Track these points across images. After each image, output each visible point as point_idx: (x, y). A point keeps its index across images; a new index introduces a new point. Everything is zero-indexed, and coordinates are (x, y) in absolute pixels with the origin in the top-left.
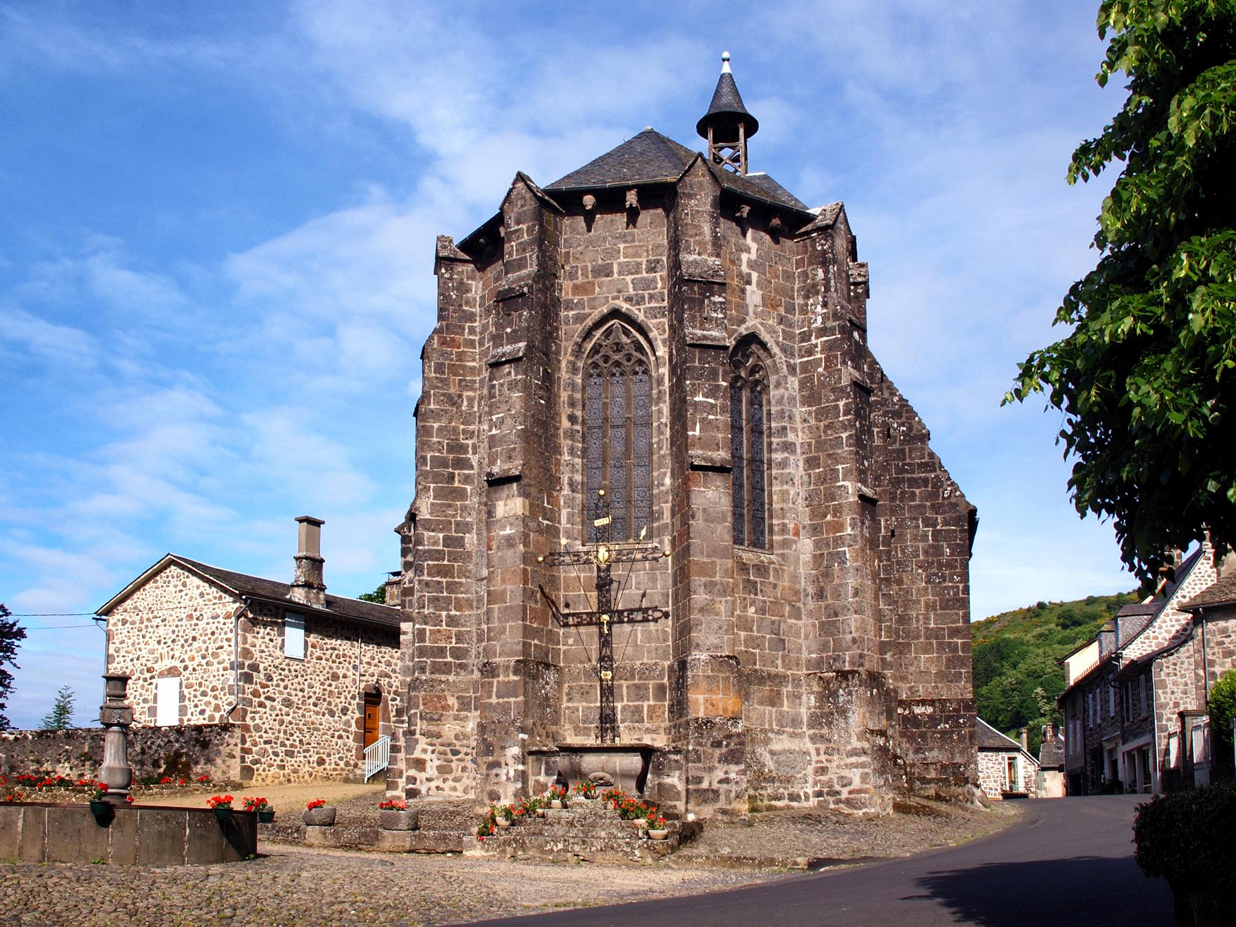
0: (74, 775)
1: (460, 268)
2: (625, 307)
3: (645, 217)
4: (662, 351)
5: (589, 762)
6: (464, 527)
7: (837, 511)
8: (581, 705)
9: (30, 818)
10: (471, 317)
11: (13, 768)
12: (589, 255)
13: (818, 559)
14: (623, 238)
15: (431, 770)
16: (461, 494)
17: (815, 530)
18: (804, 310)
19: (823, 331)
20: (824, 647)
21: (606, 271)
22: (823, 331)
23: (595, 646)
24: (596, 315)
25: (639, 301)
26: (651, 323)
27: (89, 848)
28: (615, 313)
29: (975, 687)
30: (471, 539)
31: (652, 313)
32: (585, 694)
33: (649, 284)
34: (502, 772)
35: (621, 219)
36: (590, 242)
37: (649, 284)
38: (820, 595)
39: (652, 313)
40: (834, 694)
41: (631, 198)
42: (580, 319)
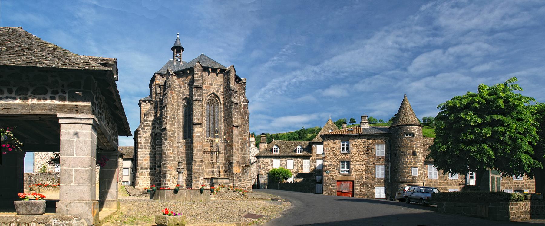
0: (51, 184)
1: (174, 77)
2: (215, 92)
3: (219, 75)
4: (222, 102)
5: (219, 181)
6: (174, 131)
7: (245, 136)
8: (208, 169)
9: (188, 192)
10: (176, 88)
11: (36, 182)
12: (208, 81)
13: (241, 144)
14: (215, 78)
15: (171, 182)
16: (174, 125)
17: (241, 139)
18: (239, 98)
19: (243, 102)
20: (243, 161)
21: (211, 84)
22: (243, 102)
23: (210, 158)
24: (210, 93)
25: (218, 92)
26: (220, 96)
27: (199, 198)
28: (213, 93)
29: (520, 171)
30: (176, 134)
31: (220, 94)
32: (208, 167)
33: (220, 89)
34: (199, 182)
35: (215, 74)
36: (209, 78)
37: (220, 89)
38: (242, 151)
39: (220, 94)
40: (245, 169)
41: (218, 71)
42: (207, 93)
